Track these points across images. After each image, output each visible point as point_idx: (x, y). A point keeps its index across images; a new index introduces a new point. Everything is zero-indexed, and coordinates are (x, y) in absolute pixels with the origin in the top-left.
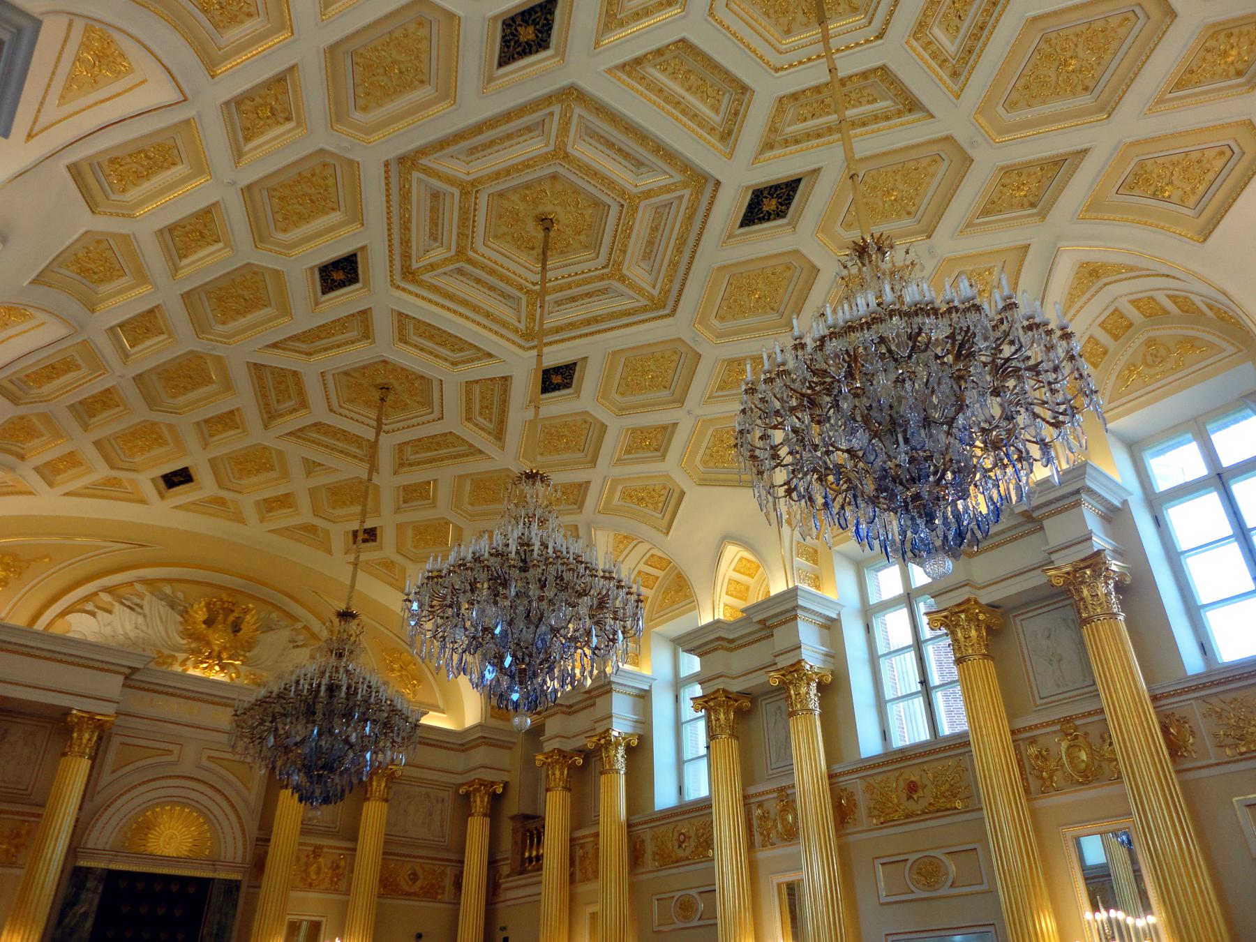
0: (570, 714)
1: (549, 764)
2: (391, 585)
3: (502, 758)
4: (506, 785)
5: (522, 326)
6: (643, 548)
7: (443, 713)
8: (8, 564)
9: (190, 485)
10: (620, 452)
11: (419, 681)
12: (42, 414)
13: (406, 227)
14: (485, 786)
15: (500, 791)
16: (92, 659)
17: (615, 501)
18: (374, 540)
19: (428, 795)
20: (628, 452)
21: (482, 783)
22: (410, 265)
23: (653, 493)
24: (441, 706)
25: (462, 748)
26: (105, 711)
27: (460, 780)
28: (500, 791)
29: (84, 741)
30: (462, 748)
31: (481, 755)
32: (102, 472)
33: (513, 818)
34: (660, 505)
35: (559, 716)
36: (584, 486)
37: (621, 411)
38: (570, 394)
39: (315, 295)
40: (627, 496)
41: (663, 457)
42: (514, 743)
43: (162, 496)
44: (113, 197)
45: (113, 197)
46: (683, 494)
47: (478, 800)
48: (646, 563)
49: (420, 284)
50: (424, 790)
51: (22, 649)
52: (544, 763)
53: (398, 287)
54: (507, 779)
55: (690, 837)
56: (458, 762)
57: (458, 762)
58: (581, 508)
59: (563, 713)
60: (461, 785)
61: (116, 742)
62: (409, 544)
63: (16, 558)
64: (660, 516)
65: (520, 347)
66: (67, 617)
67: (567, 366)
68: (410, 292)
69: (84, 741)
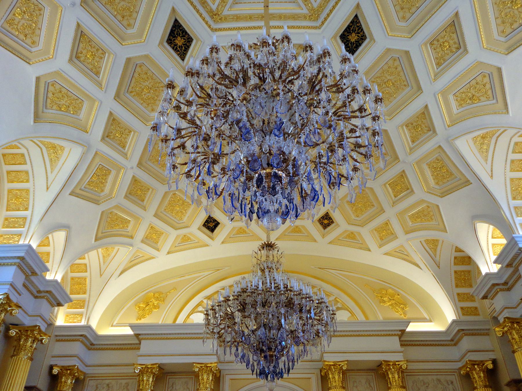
0: (509, 289)
1: (506, 332)
2: (361, 248)
3: (483, 342)
4: (494, 362)
5: (305, 11)
6: (504, 140)
7: (430, 321)
8: (157, 297)
9: (219, 226)
10: (433, 69)
11: (405, 305)
12: (115, 206)
13: (508, 199)
14: (478, 365)
15: (490, 366)
16: (198, 334)
17: (455, 111)
18: (333, 222)
19: (439, 380)
20: (438, 64)
21: (474, 363)
22: (211, 9)
23: (478, 86)
24: (428, 318)
25: (453, 343)
26: (212, 361)
27: (460, 365)
28: (490, 366)
29: (205, 380)
30: (453, 343)
31: (466, 343)
32: (173, 235)
33: (508, 384)
34: (490, 92)
35: (500, 294)
36: (425, 112)
37: (413, 32)
38: (369, 43)
39: (179, 63)
40: (461, 102)
41: (466, 51)
42: (489, 329)
43: (212, 238)
44: (33, 50)
45: (33, 50)
46: (499, 70)
47: (476, 376)
48: (514, 152)
49: (226, 19)
50: (435, 377)
51: (163, 336)
52: (503, 333)
53: (216, 30)
54: (493, 357)
55: (165, 100)
56: (454, 353)
57: (454, 353)
58: (435, 131)
59: (501, 290)
60: (460, 369)
61: (227, 378)
62: (353, 217)
63: (160, 293)
64: (495, 101)
65: (315, 28)
66: (190, 317)
67: (352, 22)
68: (225, 29)
69: (205, 380)
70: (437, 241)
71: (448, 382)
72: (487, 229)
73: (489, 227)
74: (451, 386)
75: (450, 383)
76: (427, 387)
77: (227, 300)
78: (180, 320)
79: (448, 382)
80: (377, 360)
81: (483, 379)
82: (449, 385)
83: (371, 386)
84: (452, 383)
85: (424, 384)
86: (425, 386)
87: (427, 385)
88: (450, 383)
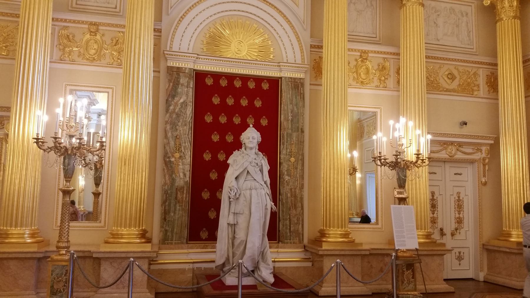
19: (453, 10)
50: (449, 6)
70: (161, 22)
71: (462, 14)
72: (427, 291)
73: (426, 291)
74: (465, 19)
75: (464, 14)
76: (438, 15)
77: (404, 161)
78: (526, 202)
79: (462, 14)
80: (217, 235)
81: (515, 9)
82: (463, 16)
83: (372, 5)
84: (467, 14)
85: (435, 12)
86: (437, 14)
87: (439, 13)
88: (464, 14)
